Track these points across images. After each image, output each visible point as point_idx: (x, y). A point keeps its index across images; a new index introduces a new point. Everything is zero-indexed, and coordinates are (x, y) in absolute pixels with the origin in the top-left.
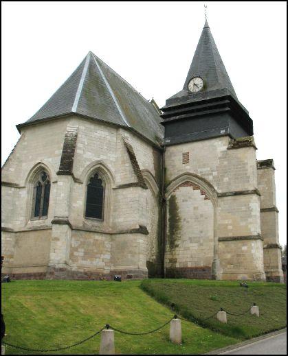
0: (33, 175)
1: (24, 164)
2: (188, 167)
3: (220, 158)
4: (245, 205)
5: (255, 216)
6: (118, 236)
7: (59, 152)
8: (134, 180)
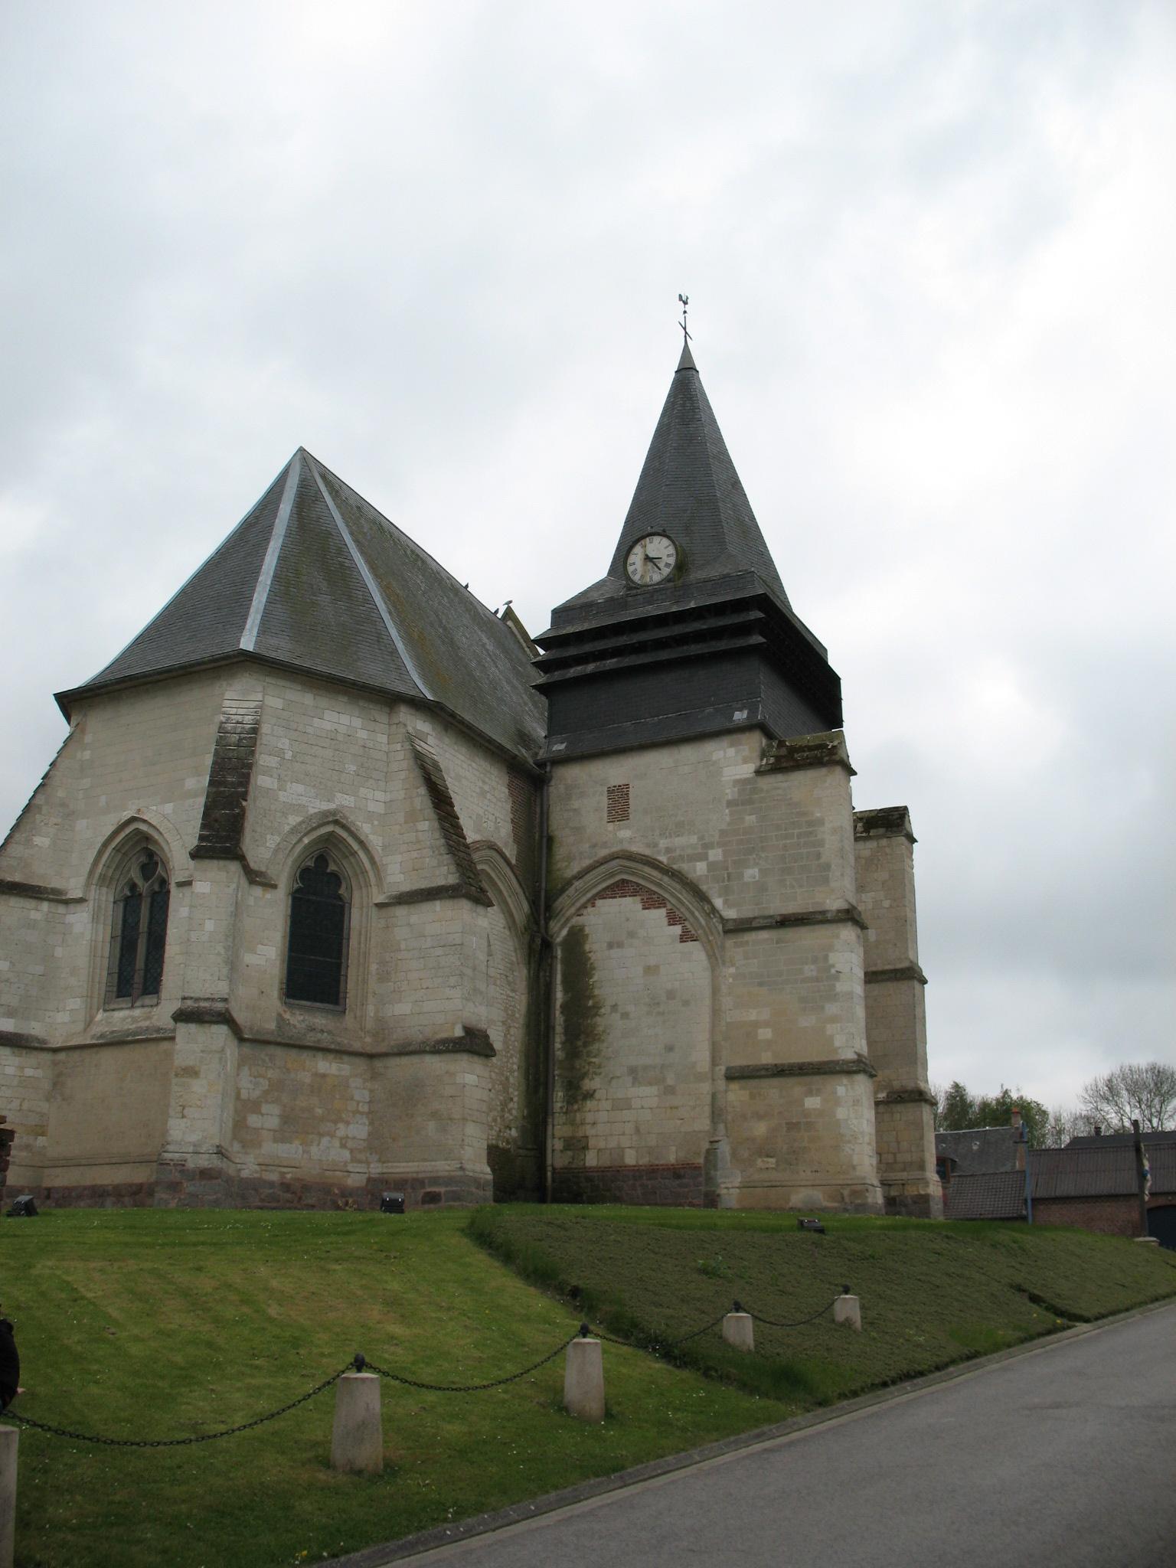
0: (111, 858)
1: (81, 824)
2: (625, 834)
3: (729, 804)
4: (815, 961)
5: (850, 995)
6: (397, 1061)
7: (198, 783)
8: (445, 874)
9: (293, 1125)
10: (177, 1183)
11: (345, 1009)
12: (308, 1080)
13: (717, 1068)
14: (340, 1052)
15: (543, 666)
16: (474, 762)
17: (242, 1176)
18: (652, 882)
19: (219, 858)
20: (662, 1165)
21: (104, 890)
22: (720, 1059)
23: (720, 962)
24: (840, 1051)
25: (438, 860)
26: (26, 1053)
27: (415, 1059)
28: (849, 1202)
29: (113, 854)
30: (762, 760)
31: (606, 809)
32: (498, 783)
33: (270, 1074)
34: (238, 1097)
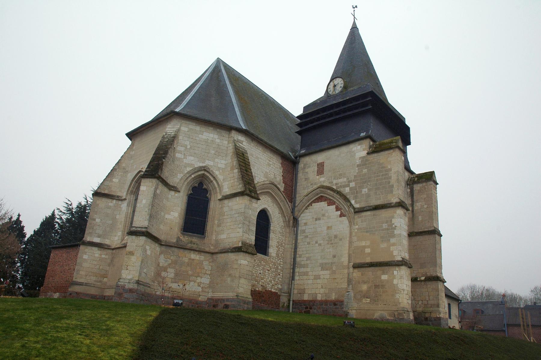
0: (134, 185)
2: (322, 179)
3: (358, 166)
4: (387, 222)
5: (400, 235)
6: (219, 255)
9: (180, 277)
10: (121, 293)
11: (205, 237)
12: (186, 261)
13: (350, 264)
14: (200, 251)
15: (299, 125)
16: (265, 153)
17: (157, 294)
18: (331, 196)
19: (150, 178)
20: (330, 300)
21: (132, 196)
22: (351, 260)
23: (353, 224)
24: (395, 257)
25: (239, 183)
26: (103, 250)
27: (226, 254)
28: (397, 317)
29: (135, 183)
30: (370, 149)
31: (316, 171)
32: (276, 162)
33: (172, 258)
34: (159, 265)
